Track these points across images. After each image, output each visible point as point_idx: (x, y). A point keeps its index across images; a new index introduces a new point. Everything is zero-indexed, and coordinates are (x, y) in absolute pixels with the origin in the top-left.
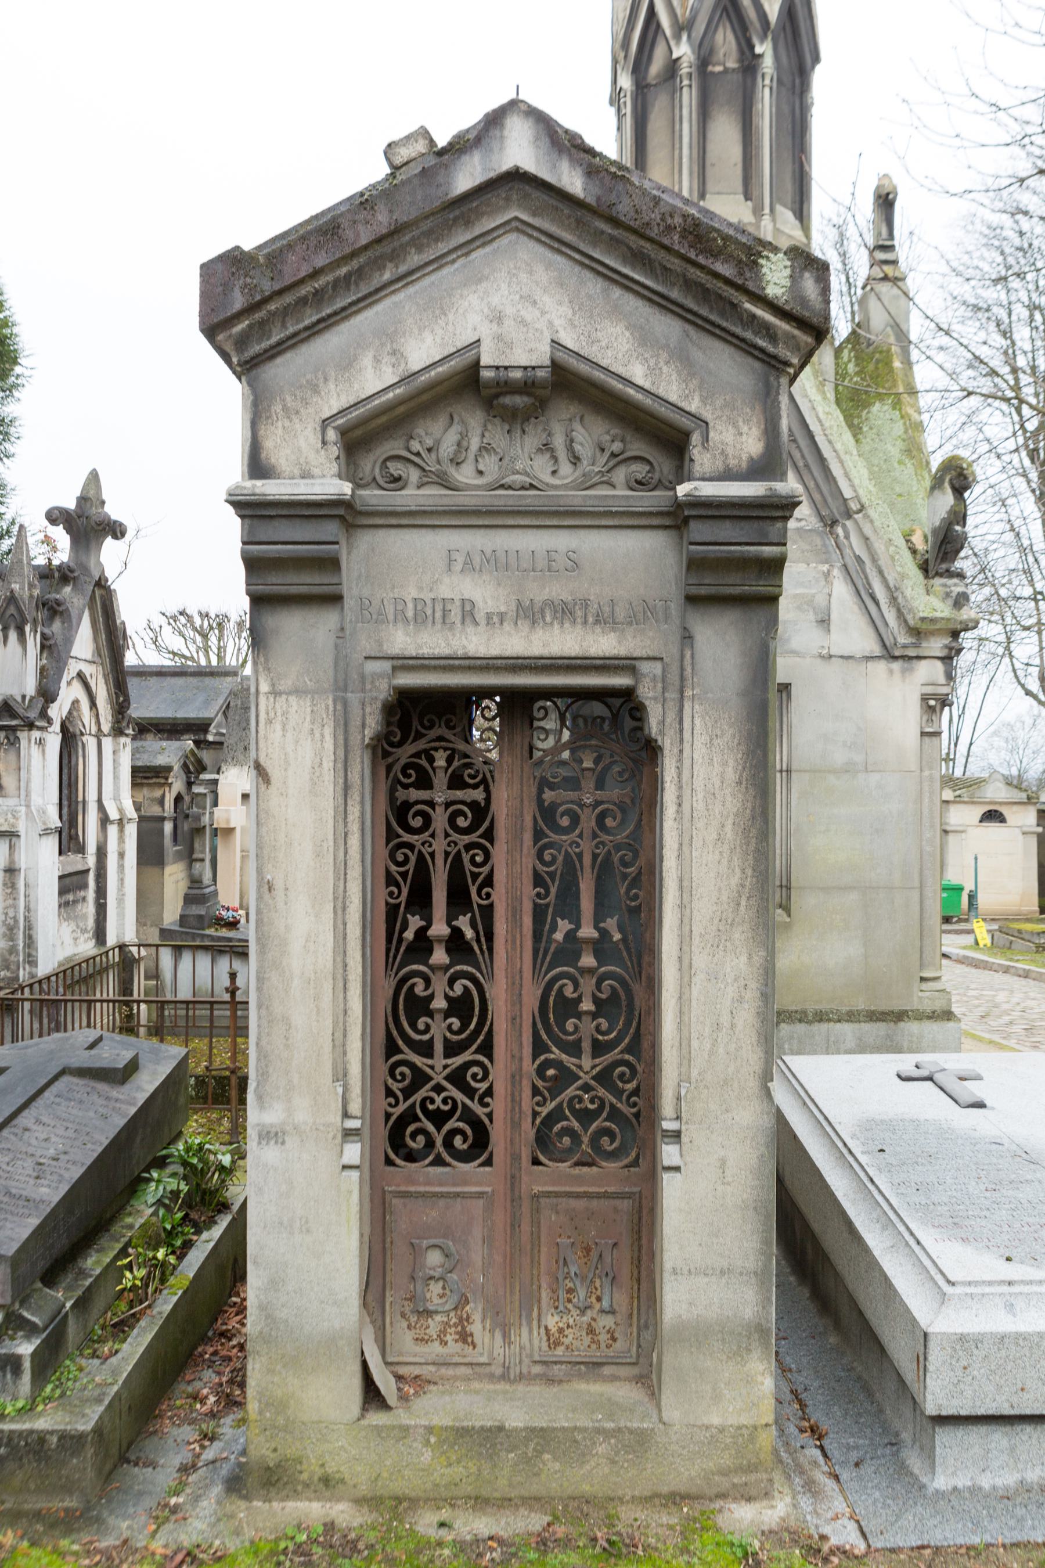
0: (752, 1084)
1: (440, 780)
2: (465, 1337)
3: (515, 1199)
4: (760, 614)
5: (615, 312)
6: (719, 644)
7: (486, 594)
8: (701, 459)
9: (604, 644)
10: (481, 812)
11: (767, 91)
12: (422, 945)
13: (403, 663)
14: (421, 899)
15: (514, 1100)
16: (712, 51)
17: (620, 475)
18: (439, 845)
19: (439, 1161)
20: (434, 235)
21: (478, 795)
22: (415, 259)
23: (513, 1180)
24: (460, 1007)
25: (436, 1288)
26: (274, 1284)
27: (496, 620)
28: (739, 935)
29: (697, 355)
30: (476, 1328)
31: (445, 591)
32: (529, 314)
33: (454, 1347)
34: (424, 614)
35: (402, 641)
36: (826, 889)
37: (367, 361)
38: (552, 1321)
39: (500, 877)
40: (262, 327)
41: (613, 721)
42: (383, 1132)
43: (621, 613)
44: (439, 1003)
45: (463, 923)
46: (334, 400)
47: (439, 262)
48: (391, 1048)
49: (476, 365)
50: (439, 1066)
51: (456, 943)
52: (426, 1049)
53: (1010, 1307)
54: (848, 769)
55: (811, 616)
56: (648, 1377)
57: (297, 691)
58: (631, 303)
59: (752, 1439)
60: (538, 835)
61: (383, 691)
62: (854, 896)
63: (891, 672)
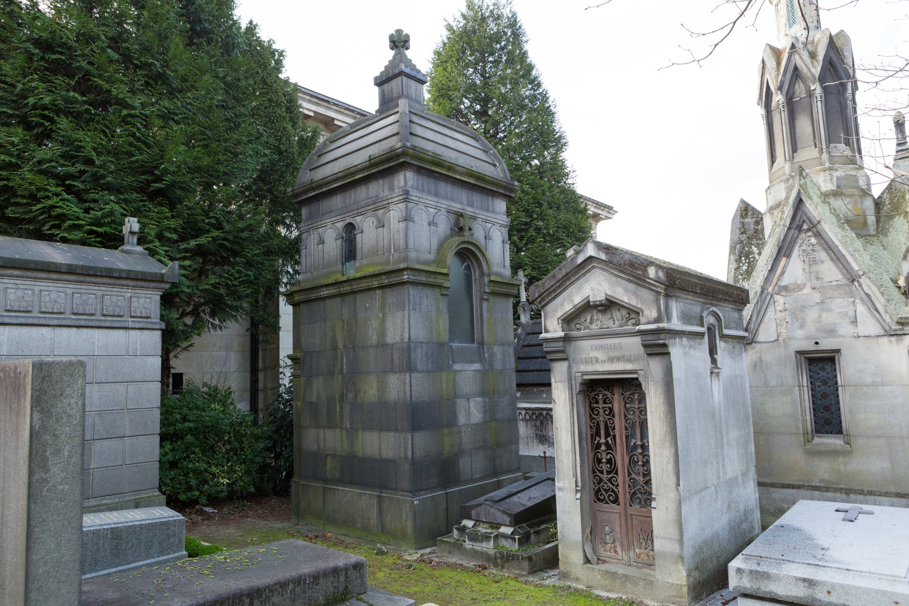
0: (673, 486)
1: (601, 402)
2: (616, 552)
3: (626, 515)
4: (666, 357)
5: (619, 284)
6: (655, 366)
7: (601, 355)
8: (643, 319)
9: (629, 367)
10: (611, 410)
11: (819, 103)
12: (598, 446)
13: (584, 374)
14: (598, 434)
15: (624, 488)
16: (794, 93)
17: (630, 322)
18: (601, 419)
19: (607, 503)
20: (576, 273)
21: (610, 405)
22: (574, 279)
23: (626, 509)
24: (609, 461)
25: (608, 537)
26: (563, 526)
27: (603, 362)
28: (667, 444)
29: (639, 293)
30: (619, 549)
31: (591, 355)
32: (600, 287)
33: (613, 554)
34: (588, 361)
35: (583, 368)
36: (868, 437)
37: (566, 303)
38: (637, 551)
39: (617, 427)
40: (543, 299)
41: (630, 385)
42: (593, 493)
43: (632, 358)
44: (604, 460)
45: (609, 439)
46: (560, 313)
47: (579, 278)
48: (594, 472)
49: (589, 302)
50: (605, 477)
51: (607, 444)
52: (602, 472)
53: (759, 564)
54: (874, 385)
55: (848, 320)
56: (651, 565)
57: (560, 381)
58: (623, 281)
59: (681, 588)
60: (625, 416)
61: (579, 380)
62: (882, 441)
63: (891, 341)
